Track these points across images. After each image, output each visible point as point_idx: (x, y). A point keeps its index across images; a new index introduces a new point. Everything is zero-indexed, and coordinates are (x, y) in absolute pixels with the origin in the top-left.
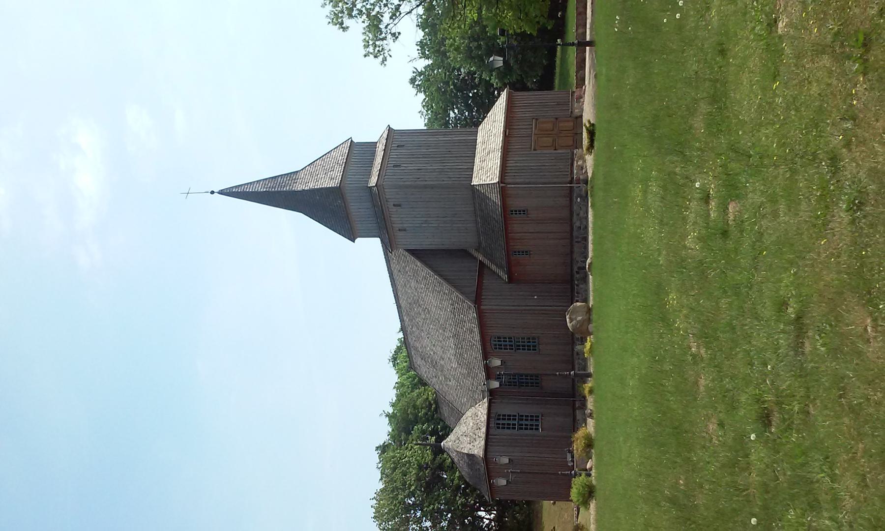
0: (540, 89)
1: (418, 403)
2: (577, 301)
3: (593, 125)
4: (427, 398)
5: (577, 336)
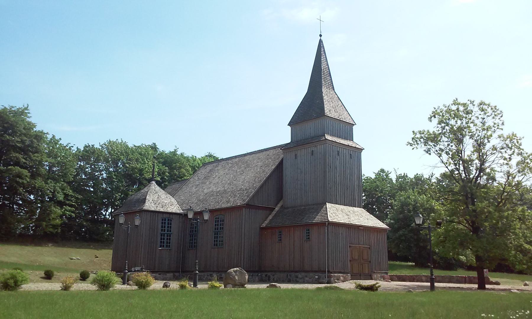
0: (389, 252)
1: (182, 170)
2: (249, 276)
3: (377, 290)
4: (185, 176)
5: (223, 275)
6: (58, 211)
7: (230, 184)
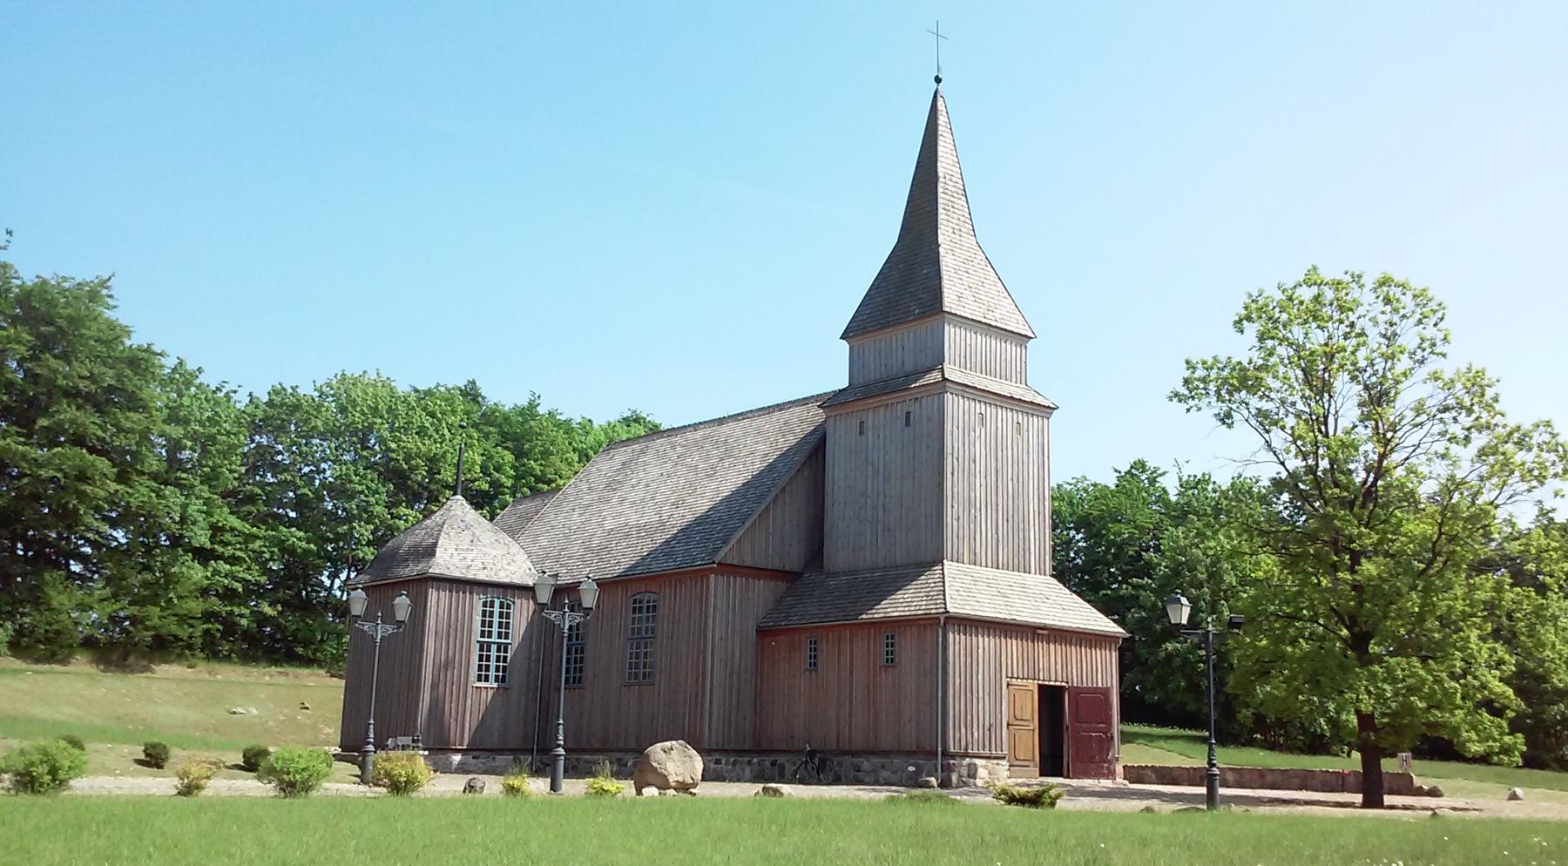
3: (1053, 804)
6: (198, 574)
7: (675, 505)
